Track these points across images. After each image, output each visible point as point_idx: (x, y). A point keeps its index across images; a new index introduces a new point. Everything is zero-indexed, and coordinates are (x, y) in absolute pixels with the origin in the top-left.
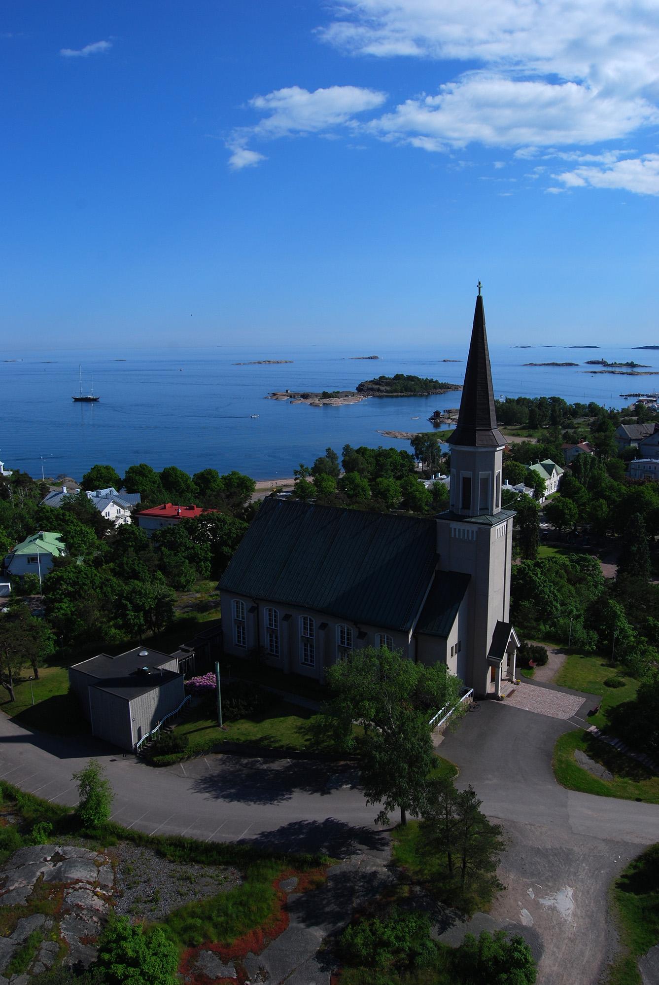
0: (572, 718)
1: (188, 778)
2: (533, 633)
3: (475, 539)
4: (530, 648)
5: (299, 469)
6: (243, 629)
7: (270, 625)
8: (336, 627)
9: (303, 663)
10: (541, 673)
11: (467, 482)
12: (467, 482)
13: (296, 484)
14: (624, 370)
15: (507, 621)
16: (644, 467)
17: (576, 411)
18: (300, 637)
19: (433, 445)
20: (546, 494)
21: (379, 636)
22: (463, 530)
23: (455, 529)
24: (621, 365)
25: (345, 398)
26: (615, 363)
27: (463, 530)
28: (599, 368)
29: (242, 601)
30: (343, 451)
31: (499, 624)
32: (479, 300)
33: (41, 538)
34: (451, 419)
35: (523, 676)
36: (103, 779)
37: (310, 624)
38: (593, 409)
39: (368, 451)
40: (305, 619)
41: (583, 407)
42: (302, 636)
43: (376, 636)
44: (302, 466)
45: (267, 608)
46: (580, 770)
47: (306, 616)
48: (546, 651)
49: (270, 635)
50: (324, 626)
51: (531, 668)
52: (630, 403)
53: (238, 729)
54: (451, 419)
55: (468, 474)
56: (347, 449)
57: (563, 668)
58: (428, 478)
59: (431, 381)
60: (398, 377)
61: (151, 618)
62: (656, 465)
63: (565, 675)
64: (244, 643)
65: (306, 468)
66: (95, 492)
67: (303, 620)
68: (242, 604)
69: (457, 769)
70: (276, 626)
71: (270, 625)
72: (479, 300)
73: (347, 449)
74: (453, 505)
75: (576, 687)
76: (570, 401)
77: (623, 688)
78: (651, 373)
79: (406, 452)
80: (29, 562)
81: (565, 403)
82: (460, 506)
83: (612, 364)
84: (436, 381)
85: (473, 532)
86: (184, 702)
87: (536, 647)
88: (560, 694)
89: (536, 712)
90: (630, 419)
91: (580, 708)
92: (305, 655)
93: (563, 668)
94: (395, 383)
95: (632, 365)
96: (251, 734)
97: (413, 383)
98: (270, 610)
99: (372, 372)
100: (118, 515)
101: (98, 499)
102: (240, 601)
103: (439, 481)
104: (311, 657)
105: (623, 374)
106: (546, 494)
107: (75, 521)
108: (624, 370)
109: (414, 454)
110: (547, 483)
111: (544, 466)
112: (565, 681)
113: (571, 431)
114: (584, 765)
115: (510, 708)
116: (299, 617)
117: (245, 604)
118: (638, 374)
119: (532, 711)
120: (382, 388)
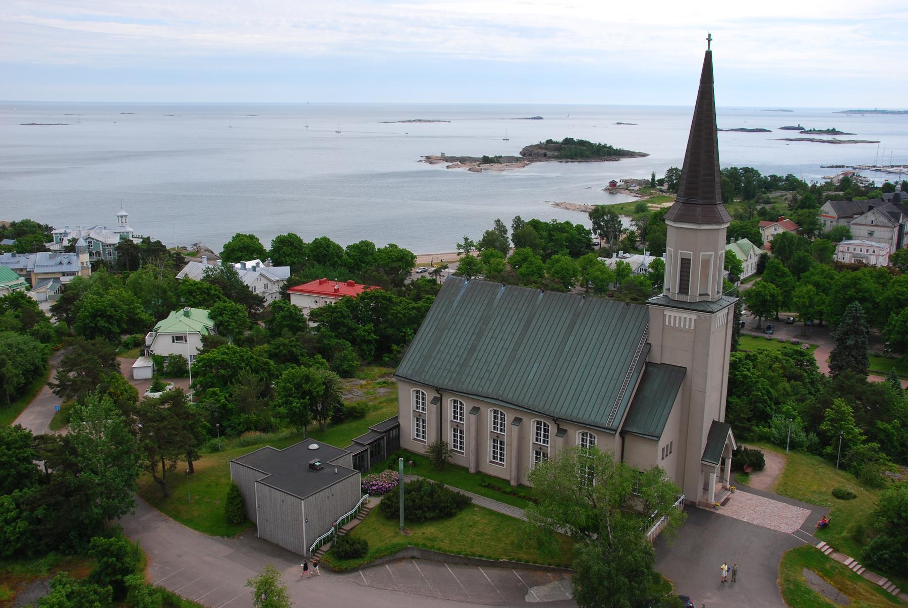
0: (797, 532)
1: (369, 586)
2: (746, 435)
3: (692, 328)
4: (744, 452)
9: (491, 462)
10: (757, 480)
13: (462, 260)
15: (722, 420)
16: (855, 250)
17: (773, 183)
19: (614, 219)
20: (742, 278)
23: (670, 316)
24: (821, 132)
25: (508, 164)
26: (814, 129)
28: (795, 134)
30: (512, 223)
31: (715, 423)
32: (708, 55)
33: (187, 315)
34: (629, 190)
35: (737, 482)
36: (280, 586)
37: (461, 408)
38: (792, 183)
39: (85, 289)
41: (780, 179)
42: (452, 421)
43: (577, 434)
44: (466, 239)
45: (414, 389)
46: (808, 592)
47: (540, 420)
48: (763, 455)
49: (454, 429)
50: (518, 421)
51: (747, 474)
52: (836, 175)
53: (423, 533)
54: (629, 190)
55: (688, 254)
56: (518, 221)
57: (782, 475)
58: (610, 256)
59: (605, 146)
60: (568, 141)
61: (317, 407)
62: (855, 247)
63: (785, 483)
64: (423, 437)
65: (471, 242)
66: (239, 264)
69: (672, 585)
70: (423, 409)
71: (537, 441)
72: (708, 55)
73: (518, 221)
74: (668, 290)
75: (799, 497)
76: (765, 174)
77: (853, 501)
78: (856, 142)
79: (582, 226)
80: (173, 342)
81: (759, 175)
82: (677, 291)
83: (811, 130)
84: (610, 147)
85: (690, 319)
86: (361, 501)
87: (751, 450)
88: (781, 505)
89: (755, 523)
90: (836, 195)
91: (806, 521)
92: (418, 430)
93: (782, 475)
94: (565, 148)
96: (438, 540)
97: (585, 148)
99: (538, 135)
100: (265, 290)
101: (245, 271)
103: (623, 260)
104: (424, 432)
105: (823, 142)
106: (742, 278)
107: (221, 295)
109: (591, 229)
110: (744, 265)
111: (741, 247)
112: (785, 490)
113: (767, 207)
114: (815, 586)
115: (724, 516)
116: (532, 421)
117: (465, 404)
118: (840, 142)
119: (750, 522)
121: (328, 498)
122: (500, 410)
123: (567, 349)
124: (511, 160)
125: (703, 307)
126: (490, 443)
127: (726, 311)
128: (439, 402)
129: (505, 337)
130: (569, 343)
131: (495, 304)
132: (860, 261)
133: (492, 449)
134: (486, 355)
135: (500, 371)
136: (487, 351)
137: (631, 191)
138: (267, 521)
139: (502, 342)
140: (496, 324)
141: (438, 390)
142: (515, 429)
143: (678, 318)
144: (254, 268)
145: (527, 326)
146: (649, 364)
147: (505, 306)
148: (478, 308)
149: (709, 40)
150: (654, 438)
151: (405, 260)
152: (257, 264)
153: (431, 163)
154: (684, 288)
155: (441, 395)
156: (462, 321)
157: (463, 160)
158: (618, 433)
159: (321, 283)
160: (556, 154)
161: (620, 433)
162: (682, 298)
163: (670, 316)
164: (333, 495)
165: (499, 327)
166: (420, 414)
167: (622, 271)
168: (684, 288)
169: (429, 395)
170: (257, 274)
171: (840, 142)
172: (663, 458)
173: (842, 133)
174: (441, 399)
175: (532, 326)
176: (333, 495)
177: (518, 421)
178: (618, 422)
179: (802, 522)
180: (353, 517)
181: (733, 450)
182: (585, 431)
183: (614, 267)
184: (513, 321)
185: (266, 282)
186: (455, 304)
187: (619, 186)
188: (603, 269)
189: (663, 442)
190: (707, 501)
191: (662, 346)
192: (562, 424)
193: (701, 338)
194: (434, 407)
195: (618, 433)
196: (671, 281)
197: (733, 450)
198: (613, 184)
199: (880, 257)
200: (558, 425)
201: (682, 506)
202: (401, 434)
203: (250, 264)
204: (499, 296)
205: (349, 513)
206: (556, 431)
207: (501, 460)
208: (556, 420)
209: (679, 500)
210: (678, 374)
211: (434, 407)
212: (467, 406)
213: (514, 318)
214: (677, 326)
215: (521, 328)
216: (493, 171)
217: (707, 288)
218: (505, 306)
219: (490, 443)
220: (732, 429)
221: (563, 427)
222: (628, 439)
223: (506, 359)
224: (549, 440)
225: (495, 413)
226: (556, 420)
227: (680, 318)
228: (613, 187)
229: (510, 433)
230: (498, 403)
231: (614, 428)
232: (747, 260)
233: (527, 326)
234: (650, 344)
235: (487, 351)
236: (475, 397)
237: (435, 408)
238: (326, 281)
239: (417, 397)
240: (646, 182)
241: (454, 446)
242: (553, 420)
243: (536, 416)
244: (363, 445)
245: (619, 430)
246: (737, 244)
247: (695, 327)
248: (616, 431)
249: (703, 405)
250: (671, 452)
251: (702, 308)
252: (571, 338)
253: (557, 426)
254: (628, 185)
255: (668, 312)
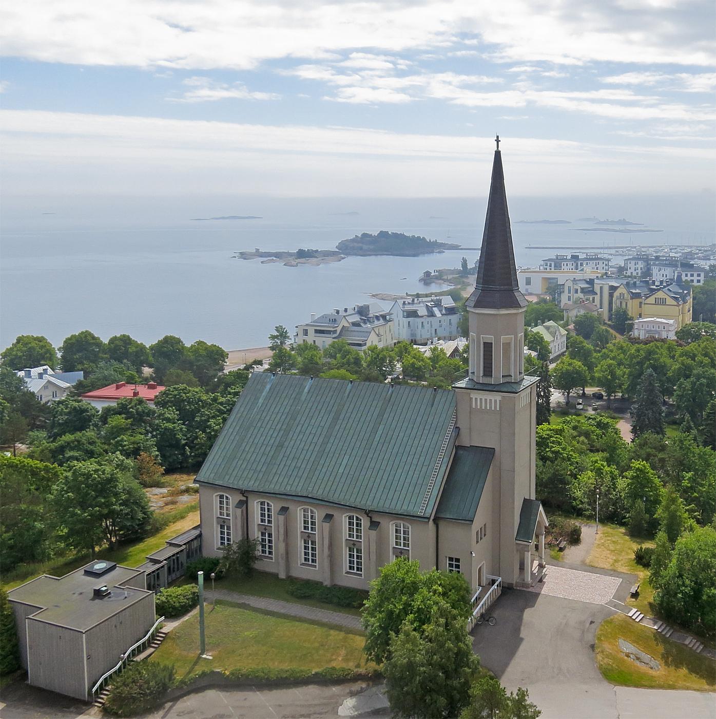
5: (276, 333)
6: (229, 528)
7: (221, 515)
8: (344, 518)
9: (347, 573)
10: (573, 553)
11: (488, 347)
12: (488, 347)
14: (617, 227)
15: (533, 497)
18: (391, 549)
21: (302, 510)
22: (490, 400)
23: (476, 399)
24: (613, 223)
27: (490, 400)
29: (227, 495)
32: (498, 155)
40: (351, 518)
42: (347, 540)
43: (390, 526)
49: (305, 541)
50: (329, 517)
55: (490, 338)
60: (383, 234)
67: (218, 499)
68: (227, 498)
70: (269, 522)
71: (305, 529)
72: (498, 155)
83: (605, 221)
85: (496, 401)
95: (623, 222)
98: (350, 518)
102: (355, 515)
105: (616, 231)
108: (617, 227)
111: (548, 328)
116: (344, 516)
118: (630, 231)
120: (365, 247)
121: (115, 627)
122: (310, 508)
123: (377, 438)
124: (327, 255)
125: (509, 387)
126: (301, 544)
127: (529, 390)
128: (245, 505)
129: (314, 431)
130: (379, 433)
131: (303, 398)
132: (653, 337)
133: (303, 550)
134: (294, 450)
135: (309, 467)
136: (296, 446)
137: (445, 280)
138: (40, 664)
139: (311, 437)
140: (304, 419)
141: (243, 492)
142: (326, 526)
143: (488, 401)
144: (41, 376)
145: (336, 419)
146: (458, 448)
147: (313, 399)
148: (285, 403)
149: (498, 141)
150: (467, 522)
151: (216, 356)
152: (45, 370)
153: (245, 259)
154: (488, 371)
155: (247, 497)
156: (268, 418)
157: (278, 255)
158: (431, 520)
159: (118, 388)
160: (372, 247)
161: (433, 520)
162: (487, 380)
163: (476, 399)
164: (121, 623)
165: (308, 421)
166: (224, 521)
167: (437, 356)
168: (488, 371)
169: (233, 499)
170: (43, 382)
171: (630, 231)
172: (477, 542)
173: (631, 224)
174: (246, 502)
175: (342, 417)
176: (121, 623)
177: (329, 517)
178: (430, 510)
179: (614, 591)
180: (144, 647)
181: (546, 527)
182: (399, 522)
183: (428, 354)
184: (322, 414)
185: (54, 389)
186: (261, 401)
187: (433, 276)
188: (418, 357)
189: (477, 525)
190: (524, 580)
191: (470, 429)
192: (374, 517)
193: (506, 416)
194: (239, 511)
195: (431, 520)
196: (476, 365)
197: (546, 527)
198: (428, 274)
199: (670, 332)
200: (371, 517)
201: (500, 589)
202: (204, 544)
203: (35, 371)
204: (306, 390)
205: (141, 641)
206: (369, 524)
207: (358, 569)
208: (368, 513)
209: (496, 584)
210: (488, 454)
211: (239, 511)
212: (319, 514)
213: (323, 411)
214: (483, 408)
215: (330, 420)
216: (307, 268)
217: (509, 369)
218: (313, 399)
219: (346, 551)
220: (543, 506)
221: (376, 519)
222: (442, 525)
223: (315, 454)
224: (362, 535)
225: (261, 504)
226: (368, 513)
227: (486, 400)
228: (427, 279)
229: (321, 532)
230: (308, 500)
231: (427, 515)
232: (554, 341)
233: (336, 419)
234: (458, 427)
235: (296, 446)
236: (283, 497)
237: (240, 512)
238: (123, 385)
239: (221, 502)
240: (459, 272)
241: (350, 567)
242: (366, 513)
243: (347, 511)
244: (159, 562)
245: (432, 518)
246: (544, 326)
247: (500, 407)
248: (429, 518)
249: (513, 484)
250: (485, 535)
251: (498, 389)
252: (381, 427)
253: (369, 518)
254: (441, 276)
255: (475, 395)
